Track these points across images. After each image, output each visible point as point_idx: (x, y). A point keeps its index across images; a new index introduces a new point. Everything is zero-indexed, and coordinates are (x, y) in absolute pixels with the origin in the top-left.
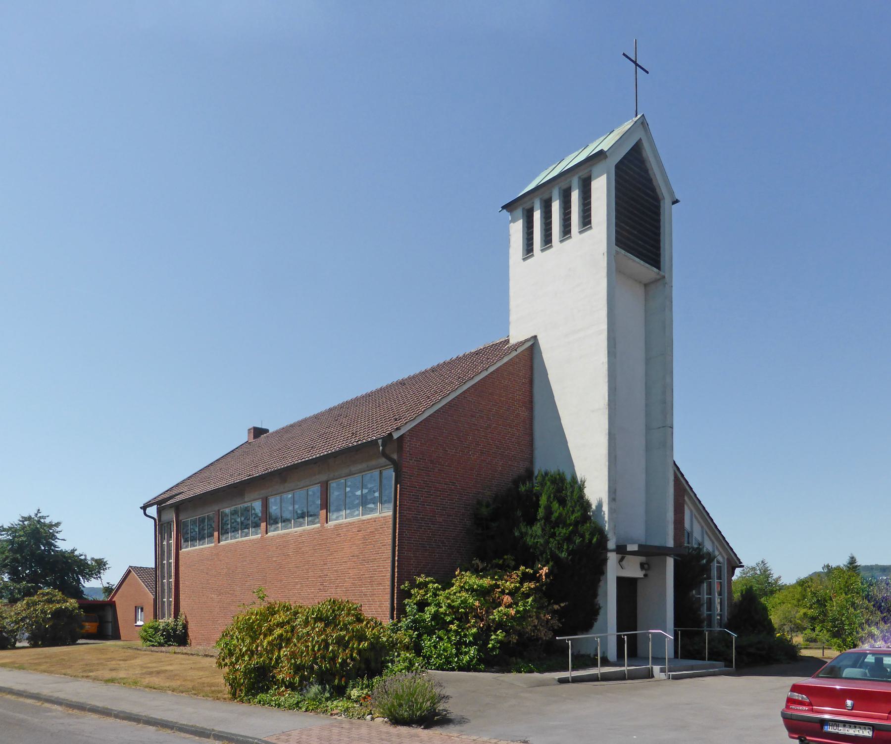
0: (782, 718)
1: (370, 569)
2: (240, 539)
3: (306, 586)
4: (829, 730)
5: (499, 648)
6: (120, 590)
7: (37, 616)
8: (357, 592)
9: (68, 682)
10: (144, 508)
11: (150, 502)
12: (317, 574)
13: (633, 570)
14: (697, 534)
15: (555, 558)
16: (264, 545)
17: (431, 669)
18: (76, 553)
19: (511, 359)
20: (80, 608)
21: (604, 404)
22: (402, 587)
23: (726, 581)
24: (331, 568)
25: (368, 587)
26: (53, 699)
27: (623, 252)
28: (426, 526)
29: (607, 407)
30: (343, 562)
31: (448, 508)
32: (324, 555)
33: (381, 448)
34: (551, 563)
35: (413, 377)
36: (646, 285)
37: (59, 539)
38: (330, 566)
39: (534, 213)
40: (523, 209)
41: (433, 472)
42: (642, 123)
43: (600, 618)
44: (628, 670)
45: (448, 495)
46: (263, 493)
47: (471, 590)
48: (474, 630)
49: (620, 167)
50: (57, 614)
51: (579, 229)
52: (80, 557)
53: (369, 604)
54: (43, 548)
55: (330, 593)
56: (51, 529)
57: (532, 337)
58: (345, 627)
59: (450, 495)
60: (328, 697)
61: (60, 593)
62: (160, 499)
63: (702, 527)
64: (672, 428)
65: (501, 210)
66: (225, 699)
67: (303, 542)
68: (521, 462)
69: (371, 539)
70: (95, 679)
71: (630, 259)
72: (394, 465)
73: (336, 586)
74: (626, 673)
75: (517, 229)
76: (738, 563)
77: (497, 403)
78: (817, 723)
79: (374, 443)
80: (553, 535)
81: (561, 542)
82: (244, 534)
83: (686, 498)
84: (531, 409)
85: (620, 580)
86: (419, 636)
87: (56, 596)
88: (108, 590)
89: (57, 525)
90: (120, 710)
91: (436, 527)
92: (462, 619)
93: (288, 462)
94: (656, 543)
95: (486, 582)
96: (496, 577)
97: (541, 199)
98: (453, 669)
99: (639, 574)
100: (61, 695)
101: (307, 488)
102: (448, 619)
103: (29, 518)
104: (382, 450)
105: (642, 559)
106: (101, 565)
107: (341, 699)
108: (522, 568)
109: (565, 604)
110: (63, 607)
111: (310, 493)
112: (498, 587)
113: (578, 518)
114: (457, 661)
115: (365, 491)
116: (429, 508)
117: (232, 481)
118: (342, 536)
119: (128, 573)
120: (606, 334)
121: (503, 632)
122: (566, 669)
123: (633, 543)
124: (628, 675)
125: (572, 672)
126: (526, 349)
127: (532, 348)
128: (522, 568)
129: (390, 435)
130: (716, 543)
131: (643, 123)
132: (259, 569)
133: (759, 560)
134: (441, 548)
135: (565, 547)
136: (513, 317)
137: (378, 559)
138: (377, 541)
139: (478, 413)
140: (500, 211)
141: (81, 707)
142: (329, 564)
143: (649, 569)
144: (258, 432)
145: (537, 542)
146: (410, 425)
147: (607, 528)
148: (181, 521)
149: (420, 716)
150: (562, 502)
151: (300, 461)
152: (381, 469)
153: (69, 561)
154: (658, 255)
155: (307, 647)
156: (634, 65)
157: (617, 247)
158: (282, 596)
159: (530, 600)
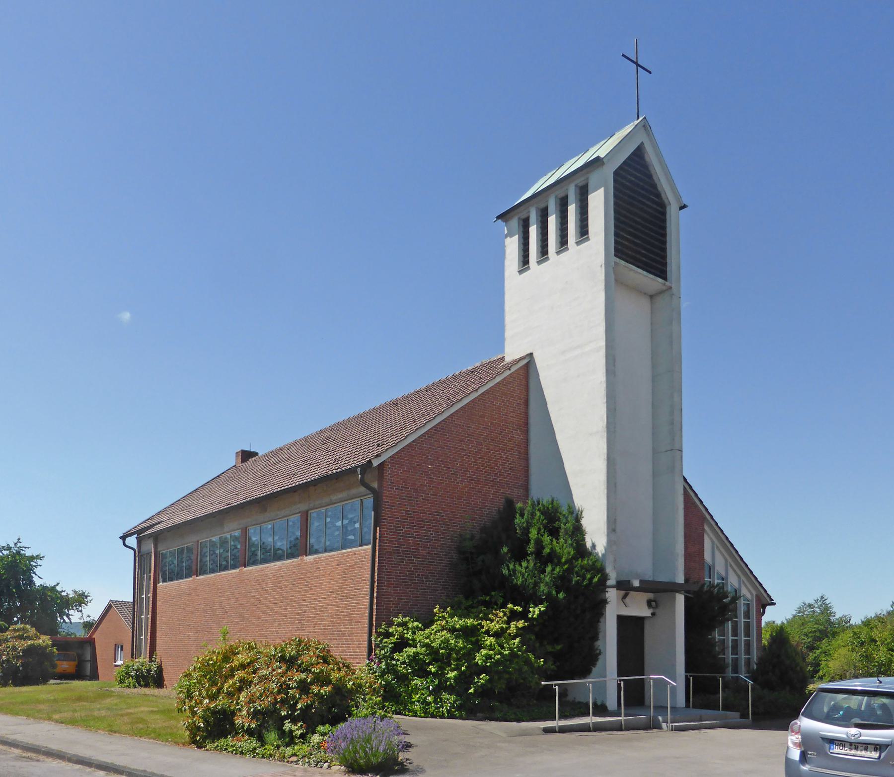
1: (349, 606)
3: (283, 624)
9: (29, 724)
10: (123, 538)
11: (130, 531)
12: (295, 610)
13: (638, 608)
14: (720, 568)
19: (504, 379)
20: (53, 645)
21: (603, 427)
23: (755, 621)
24: (310, 604)
25: (347, 625)
26: (10, 741)
27: (623, 263)
29: (606, 429)
30: (322, 598)
31: (432, 540)
33: (360, 476)
35: (407, 397)
38: (308, 602)
40: (519, 218)
41: (417, 501)
42: (644, 126)
43: (599, 663)
47: (452, 630)
50: (30, 651)
51: (576, 240)
53: (347, 644)
55: (308, 632)
57: (527, 355)
58: (307, 670)
59: (435, 526)
62: (140, 528)
63: (726, 560)
64: (681, 451)
65: (496, 220)
67: (281, 576)
68: (515, 489)
69: (350, 574)
71: (631, 270)
73: (314, 624)
74: (623, 723)
79: (352, 471)
83: (706, 527)
84: (526, 432)
85: (622, 620)
88: (88, 626)
90: (74, 753)
93: (268, 491)
94: (663, 578)
97: (537, 208)
99: (645, 612)
100: (19, 738)
101: (286, 518)
104: (361, 478)
105: (650, 596)
106: (81, 599)
108: (510, 606)
111: (291, 523)
115: (346, 522)
116: (412, 540)
117: (211, 510)
118: (321, 570)
119: (109, 607)
120: (604, 351)
122: (553, 719)
124: (624, 725)
126: (521, 368)
128: (510, 606)
129: (370, 462)
130: (743, 578)
132: (237, 605)
133: (818, 596)
134: (424, 584)
136: (508, 334)
137: (358, 595)
140: (495, 222)
141: (36, 750)
142: (308, 600)
143: (657, 606)
144: (246, 456)
146: (392, 451)
148: (160, 552)
151: (279, 489)
152: (362, 498)
156: (638, 63)
158: (260, 634)
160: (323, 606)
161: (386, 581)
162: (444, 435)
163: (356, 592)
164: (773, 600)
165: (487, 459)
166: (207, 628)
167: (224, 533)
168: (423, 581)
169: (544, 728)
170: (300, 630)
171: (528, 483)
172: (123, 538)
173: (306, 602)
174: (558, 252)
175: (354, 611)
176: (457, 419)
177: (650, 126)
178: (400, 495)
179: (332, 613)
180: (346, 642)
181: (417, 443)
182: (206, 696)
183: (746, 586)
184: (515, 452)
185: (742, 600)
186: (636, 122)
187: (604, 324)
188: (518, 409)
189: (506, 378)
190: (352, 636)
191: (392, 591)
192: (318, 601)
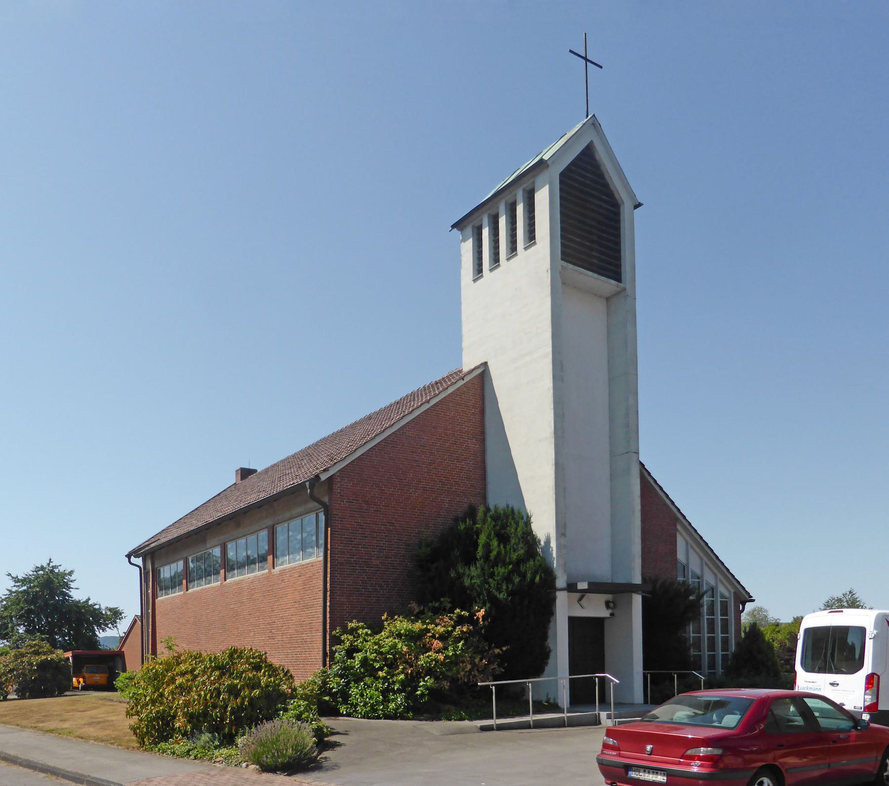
0: (597, 764)
1: (309, 615)
2: (204, 587)
3: (258, 633)
4: (632, 775)
5: (428, 694)
6: (128, 640)
7: (24, 668)
8: (299, 639)
11: (140, 546)
15: (493, 600)
16: (223, 592)
17: (358, 717)
18: (90, 603)
22: (334, 633)
24: (278, 615)
25: (308, 633)
27: (571, 266)
28: (361, 570)
32: (271, 602)
33: (309, 490)
34: (488, 605)
36: (608, 299)
37: (72, 588)
38: (277, 613)
39: (483, 231)
41: (368, 513)
42: (593, 124)
43: (551, 661)
44: (568, 717)
46: (222, 538)
48: (402, 676)
49: (566, 177)
50: (43, 666)
52: (94, 607)
54: (57, 598)
55: (277, 641)
56: (65, 579)
57: (482, 364)
58: (239, 677)
60: (218, 745)
61: (48, 645)
63: (701, 559)
66: (133, 748)
67: (254, 589)
72: (324, 508)
73: (282, 633)
75: (468, 247)
76: (747, 597)
77: (442, 437)
78: (621, 768)
79: (302, 486)
80: (492, 575)
81: (500, 582)
82: (207, 582)
83: (679, 527)
84: (483, 442)
85: (573, 621)
86: (348, 684)
87: (43, 647)
89: (71, 573)
91: (373, 570)
92: (392, 665)
94: (621, 580)
95: (418, 626)
96: (427, 621)
98: (378, 718)
99: (604, 613)
102: (377, 665)
103: (42, 568)
105: (609, 597)
107: (231, 747)
108: (458, 610)
109: (506, 647)
110: (49, 659)
112: (428, 631)
113: (521, 556)
114: (382, 709)
121: (430, 678)
123: (583, 580)
125: (496, 720)
127: (482, 375)
128: (458, 610)
130: (719, 576)
131: (594, 124)
133: (847, 590)
135: (504, 587)
136: (465, 344)
137: (316, 604)
138: (314, 586)
139: (419, 448)
140: (450, 231)
143: (615, 607)
144: (245, 473)
145: (475, 583)
147: (555, 565)
148: (157, 568)
149: (282, 763)
150: (503, 539)
152: (317, 512)
153: (83, 611)
154: (619, 266)
155: (200, 695)
156: (584, 61)
157: (563, 262)
159: (460, 644)
160: (289, 616)
161: (338, 590)
162: (395, 447)
163: (314, 602)
164: (752, 597)
165: (441, 469)
166: (197, 639)
167: (207, 549)
169: (480, 726)
170: (271, 639)
171: (485, 491)
172: (129, 556)
173: (275, 613)
174: (509, 258)
175: (314, 620)
176: (408, 431)
177: (600, 124)
178: (350, 508)
179: (296, 622)
180: (308, 649)
181: (367, 456)
183: (723, 584)
184: (471, 461)
185: (719, 598)
186: (585, 120)
187: (550, 330)
188: (473, 418)
189: (459, 388)
190: (312, 644)
191: (345, 600)
192: (284, 611)
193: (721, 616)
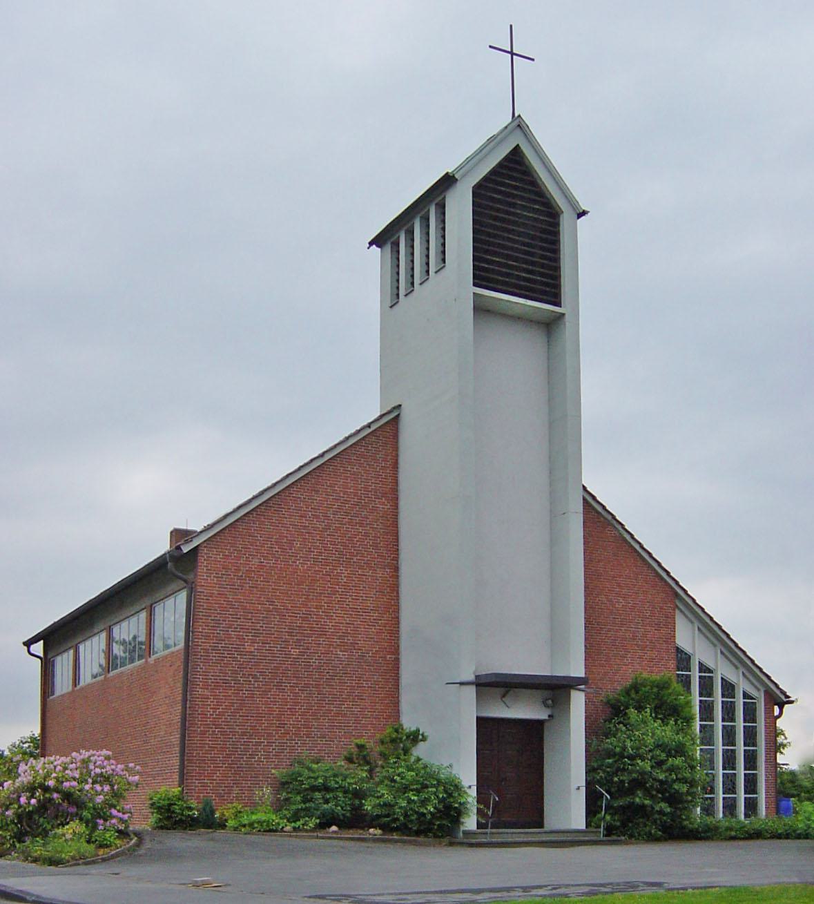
10: (28, 644)
41: (242, 589)
45: (263, 617)
70: (725, 886)
131: (518, 125)
156: (514, 51)
161: (201, 682)
168: (250, 681)
182: (132, 836)
193: (700, 721)
